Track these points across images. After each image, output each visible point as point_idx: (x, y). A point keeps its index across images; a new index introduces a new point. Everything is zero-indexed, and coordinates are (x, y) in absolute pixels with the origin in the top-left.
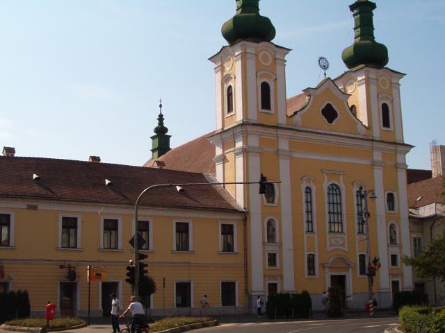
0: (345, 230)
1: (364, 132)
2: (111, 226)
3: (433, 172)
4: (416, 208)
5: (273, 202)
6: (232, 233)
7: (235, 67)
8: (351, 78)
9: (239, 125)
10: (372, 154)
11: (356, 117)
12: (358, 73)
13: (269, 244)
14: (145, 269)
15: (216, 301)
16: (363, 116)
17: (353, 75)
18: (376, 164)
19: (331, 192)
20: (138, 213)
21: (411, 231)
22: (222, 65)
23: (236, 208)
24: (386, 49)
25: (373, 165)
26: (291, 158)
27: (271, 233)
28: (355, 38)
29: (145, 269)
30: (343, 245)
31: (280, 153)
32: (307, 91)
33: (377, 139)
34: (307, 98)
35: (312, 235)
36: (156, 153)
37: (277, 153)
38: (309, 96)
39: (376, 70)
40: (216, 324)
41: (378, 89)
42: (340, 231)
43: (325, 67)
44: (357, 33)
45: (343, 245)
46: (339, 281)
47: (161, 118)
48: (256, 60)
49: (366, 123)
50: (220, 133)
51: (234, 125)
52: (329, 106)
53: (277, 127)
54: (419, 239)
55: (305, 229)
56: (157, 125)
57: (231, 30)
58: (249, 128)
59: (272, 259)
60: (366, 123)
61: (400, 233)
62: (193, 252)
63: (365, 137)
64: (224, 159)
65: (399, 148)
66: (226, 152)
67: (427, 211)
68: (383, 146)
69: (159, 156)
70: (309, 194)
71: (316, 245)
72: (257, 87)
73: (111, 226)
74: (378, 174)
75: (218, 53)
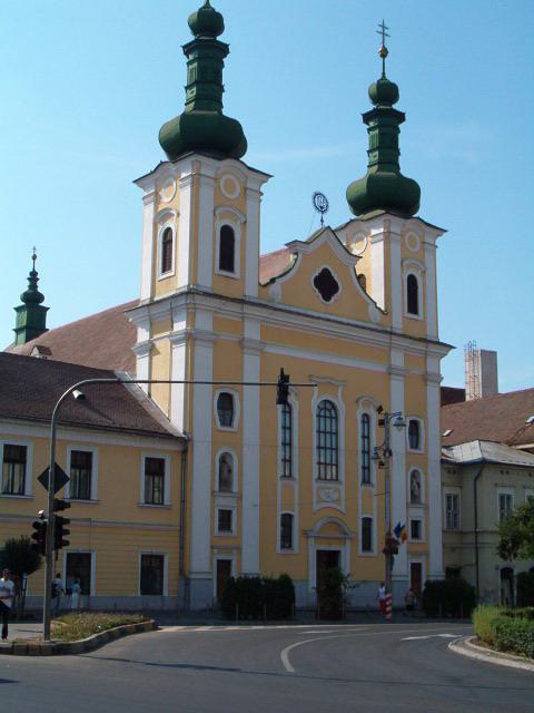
0: (342, 477)
1: (379, 318)
3: (467, 392)
4: (447, 447)
5: (230, 424)
6: (161, 474)
7: (180, 197)
8: (361, 231)
9: (182, 294)
10: (243, 326)
11: (364, 289)
12: (371, 222)
13: (222, 494)
14: (65, 527)
15: (129, 584)
16: (376, 291)
17: (364, 226)
18: (395, 371)
19: (322, 414)
20: (57, 437)
21: (443, 484)
22: (156, 193)
23: (171, 432)
24: (238, 122)
25: (390, 374)
26: (263, 355)
28: (369, 166)
29: (65, 527)
30: (338, 501)
31: (246, 344)
32: (293, 246)
33: (398, 332)
34: (292, 257)
35: (337, 486)
36: (23, 336)
37: (241, 343)
38: (296, 254)
39: (402, 221)
40: (155, 627)
41: (402, 251)
42: (334, 477)
43: (322, 210)
44: (373, 159)
45: (338, 501)
46: (328, 560)
47: (33, 277)
48: (402, 246)
49: (381, 305)
50: (147, 305)
51: (172, 293)
52: (326, 273)
53: (242, 302)
54: (456, 497)
55: (280, 473)
56: (27, 289)
57: (177, 135)
58: (199, 300)
59: (225, 519)
60: (381, 305)
61: (426, 486)
62: (97, 503)
63: (380, 328)
64: (151, 349)
65: (432, 348)
66: (155, 337)
67: (467, 452)
68: (406, 343)
69: (27, 340)
71: (296, 501)
72: (214, 233)
74: (397, 388)
75: (152, 173)
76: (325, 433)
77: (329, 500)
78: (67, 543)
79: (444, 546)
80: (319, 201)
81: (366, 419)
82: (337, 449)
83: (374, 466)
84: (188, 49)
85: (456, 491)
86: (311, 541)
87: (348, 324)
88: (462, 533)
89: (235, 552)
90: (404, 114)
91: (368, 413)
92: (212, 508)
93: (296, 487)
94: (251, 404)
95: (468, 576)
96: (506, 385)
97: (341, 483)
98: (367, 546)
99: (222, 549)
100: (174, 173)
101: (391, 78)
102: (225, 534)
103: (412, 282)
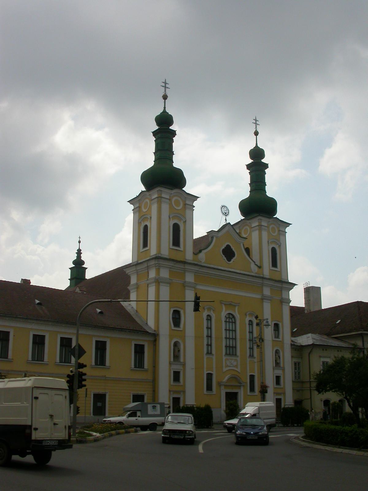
2: (39, 341)
6: (143, 352)
19: (228, 320)
21: (292, 357)
27: (176, 353)
30: (236, 366)
35: (234, 358)
39: (267, 220)
43: (226, 214)
47: (79, 252)
52: (228, 247)
54: (299, 363)
56: (76, 258)
58: (161, 262)
59: (177, 376)
62: (108, 368)
65: (285, 286)
70: (209, 321)
72: (169, 227)
73: (39, 341)
74: (267, 307)
75: (137, 197)
76: (229, 330)
77: (231, 365)
78: (85, 386)
79: (293, 389)
80: (224, 210)
81: (251, 323)
82: (235, 339)
83: (255, 347)
84: (249, 167)
85: (299, 360)
86: (223, 387)
87: (240, 274)
88: (303, 382)
89: (282, 395)
90: (268, 164)
91: (210, 314)
92: (170, 370)
93: (214, 360)
94: (189, 315)
95: (306, 405)
96: (326, 304)
97: (238, 356)
98: (252, 389)
99: (175, 392)
100: (149, 197)
101: (169, 111)
102: (176, 384)
103: (274, 251)
